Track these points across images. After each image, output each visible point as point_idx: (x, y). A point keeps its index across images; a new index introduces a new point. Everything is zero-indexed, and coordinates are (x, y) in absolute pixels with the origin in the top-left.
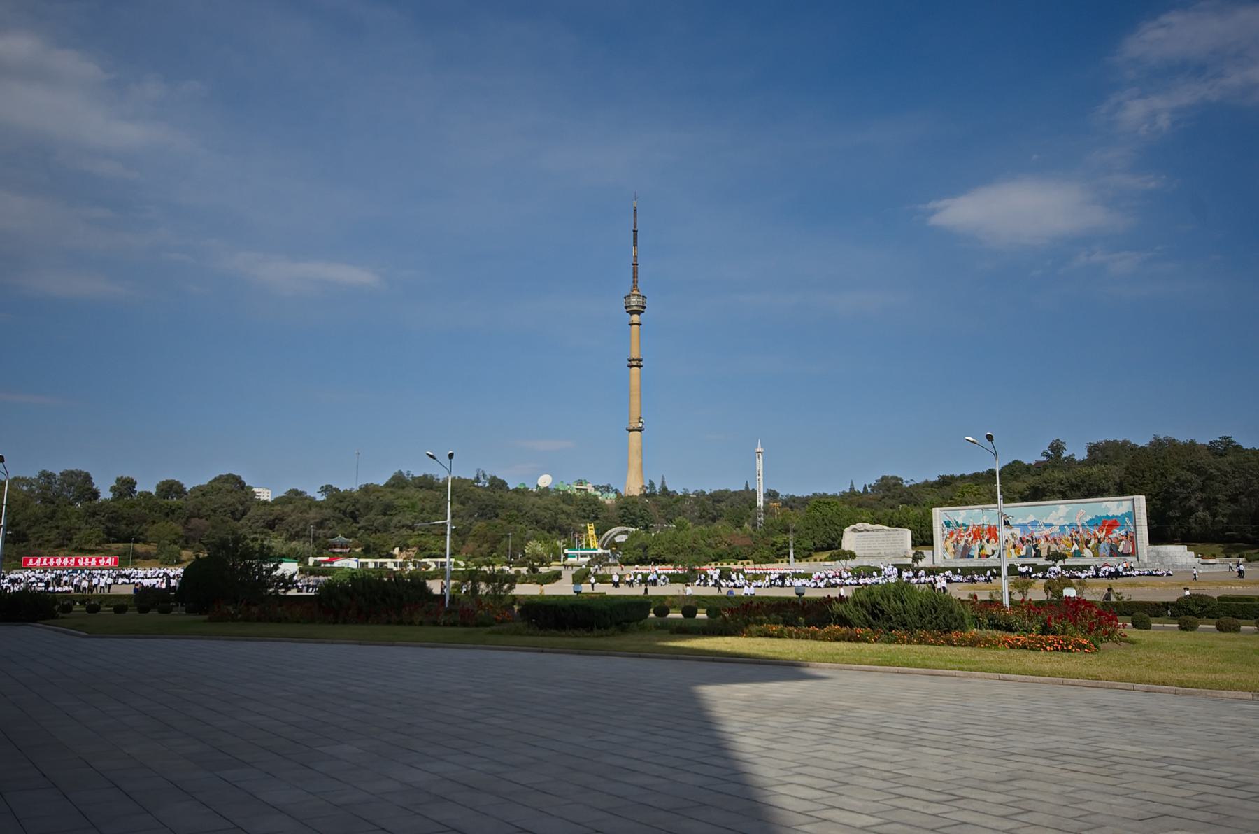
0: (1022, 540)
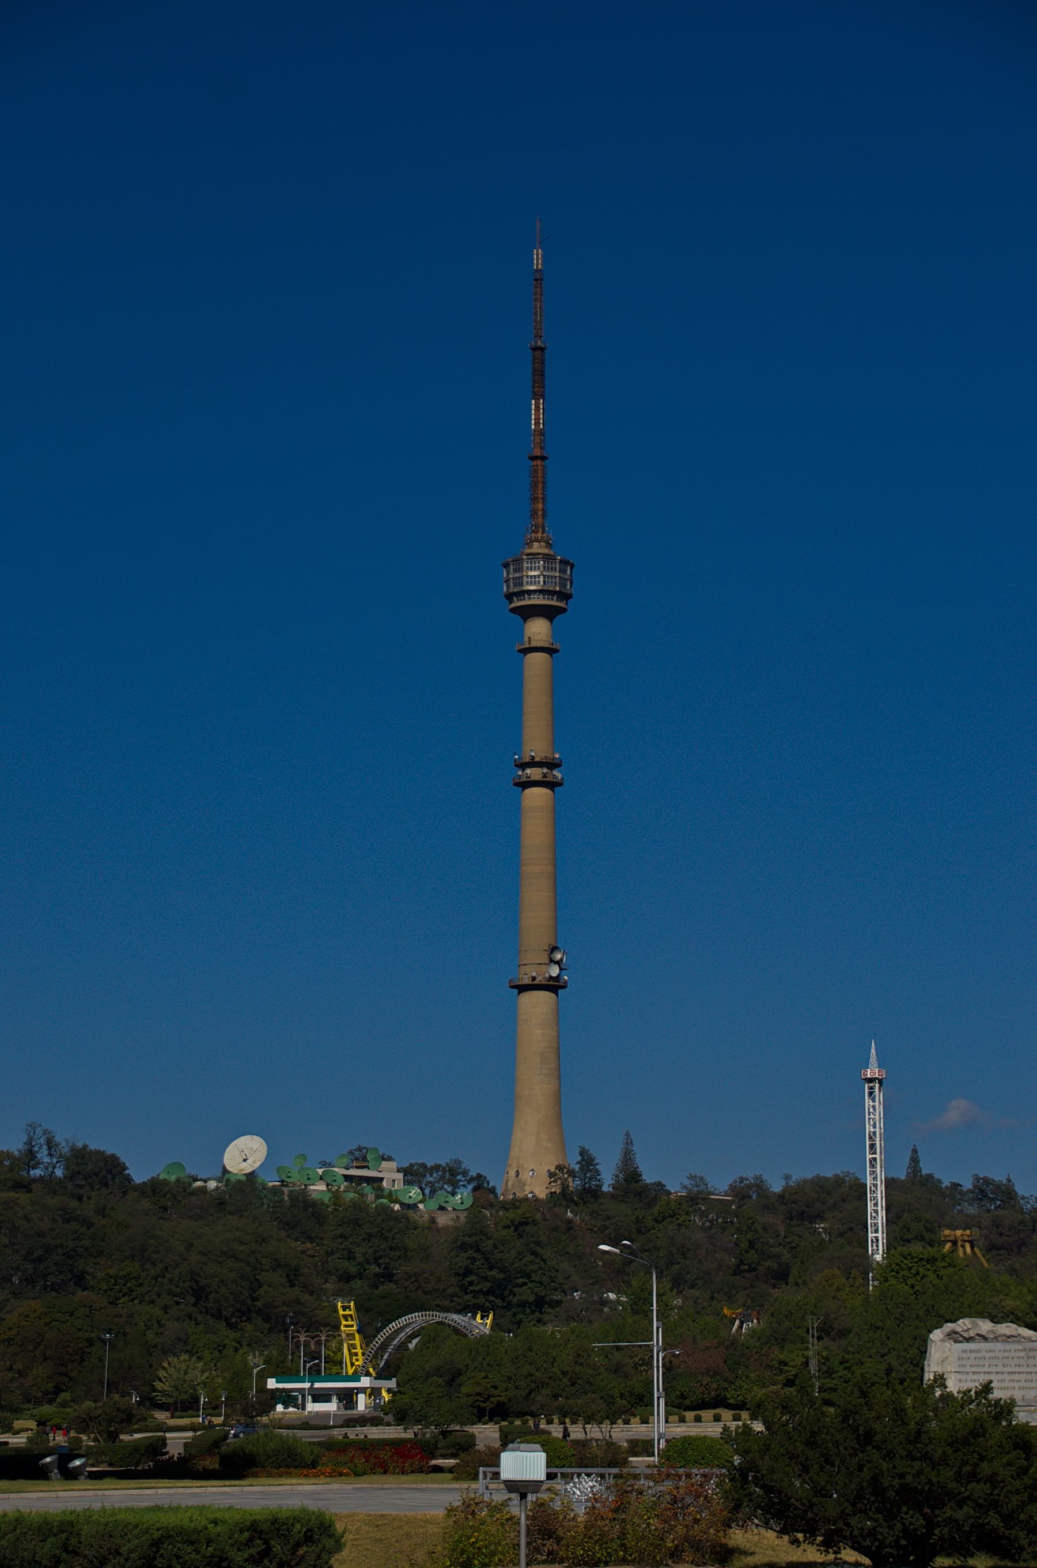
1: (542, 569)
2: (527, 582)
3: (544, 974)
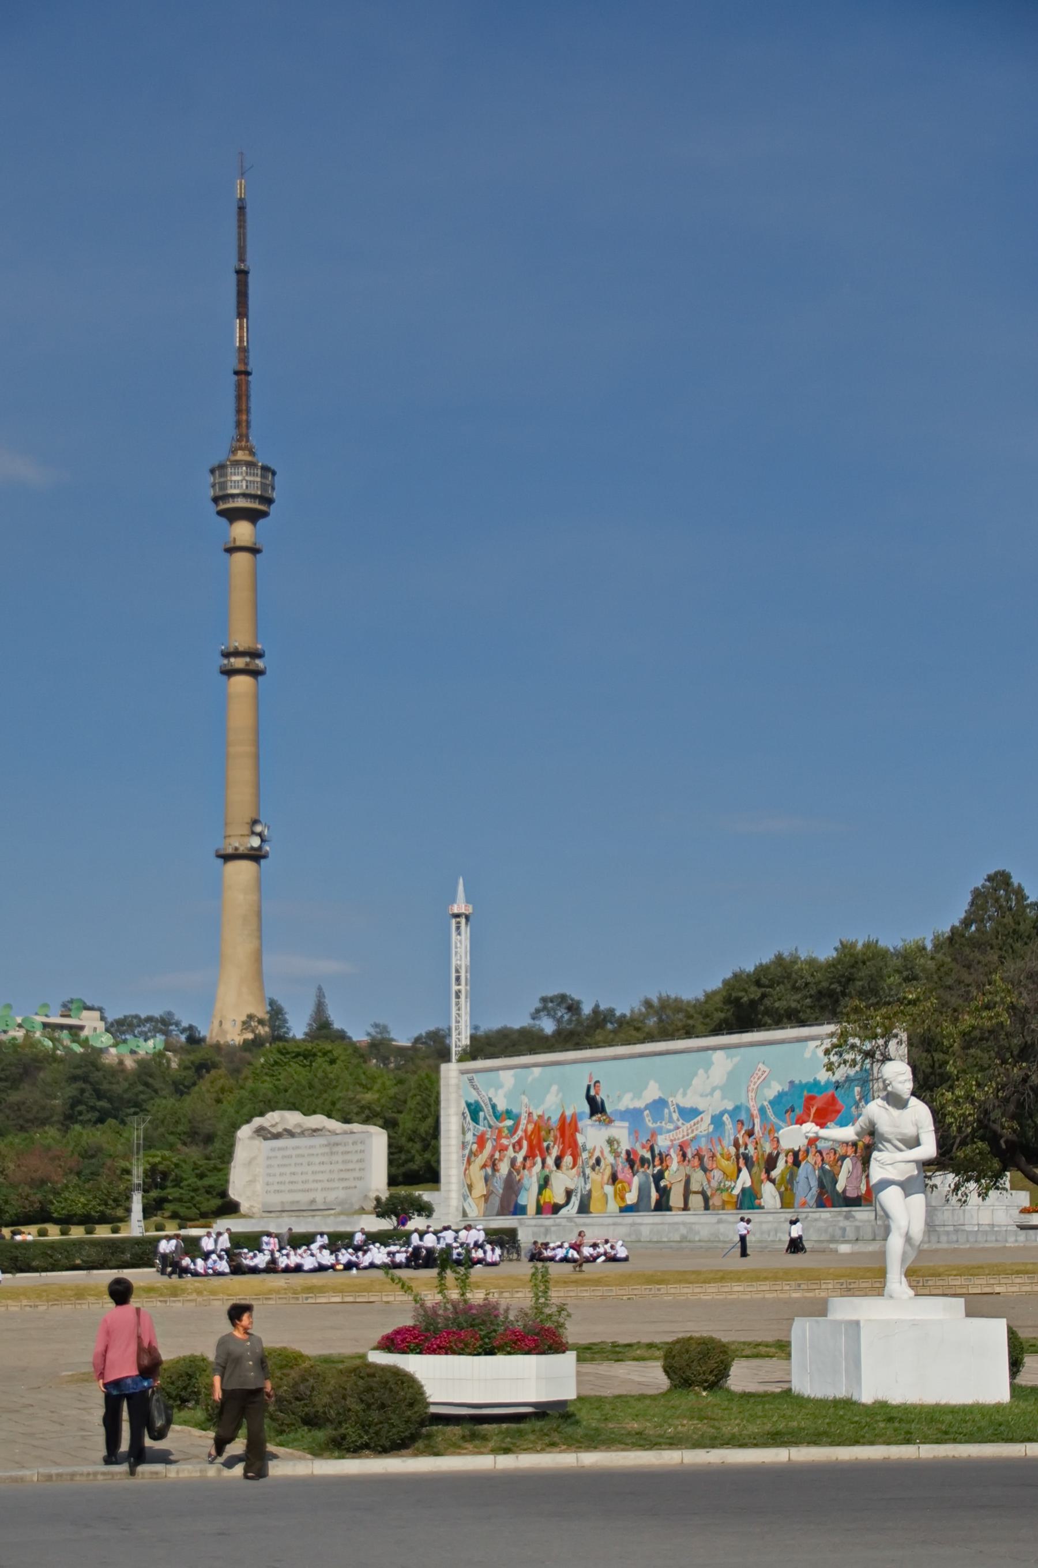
0: (632, 1161)
1: (244, 475)
2: (231, 487)
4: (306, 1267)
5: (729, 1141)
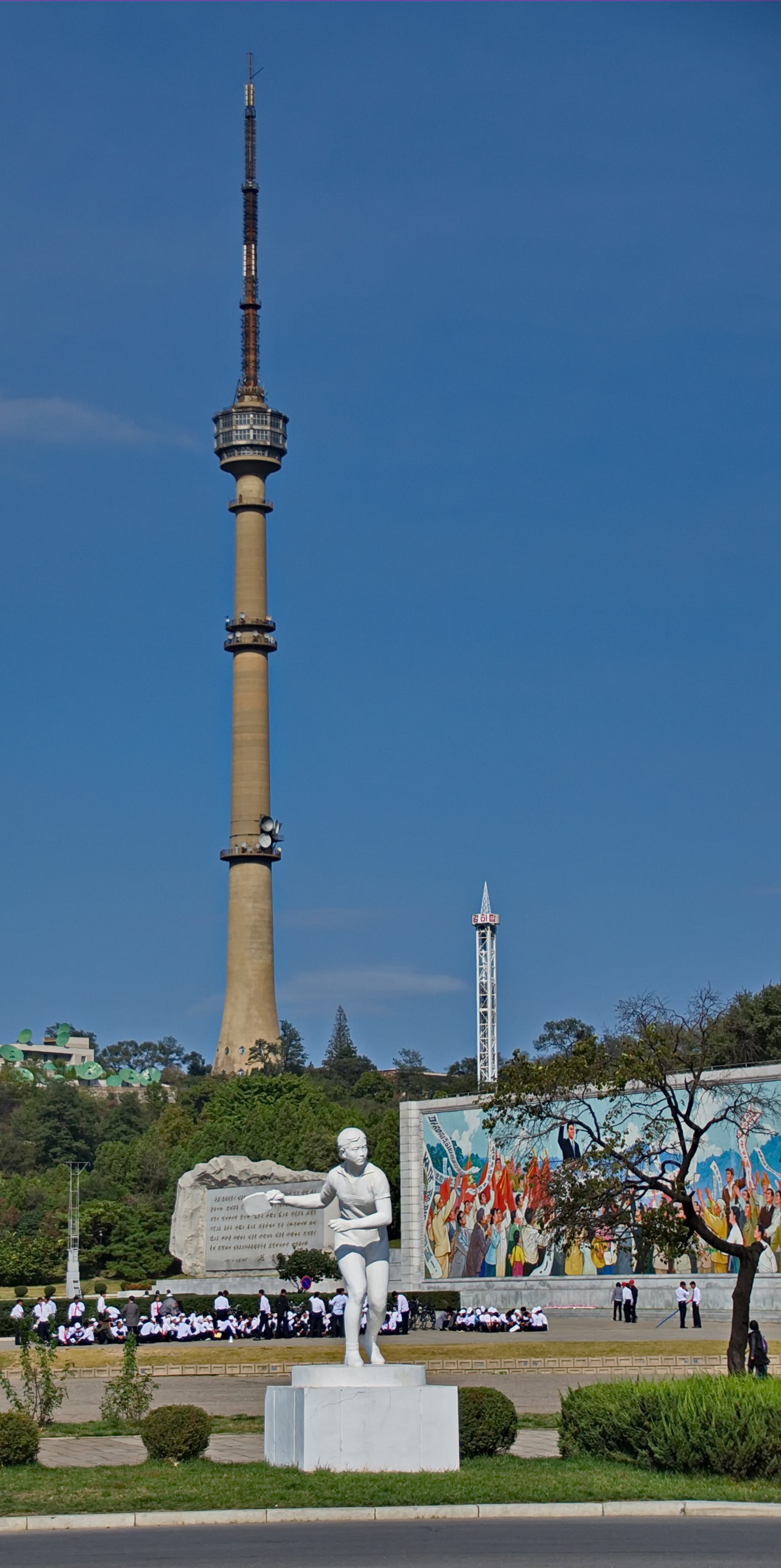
1: (252, 423)
2: (237, 437)
3: (255, 845)
4: (179, 1336)
5: (718, 1192)
